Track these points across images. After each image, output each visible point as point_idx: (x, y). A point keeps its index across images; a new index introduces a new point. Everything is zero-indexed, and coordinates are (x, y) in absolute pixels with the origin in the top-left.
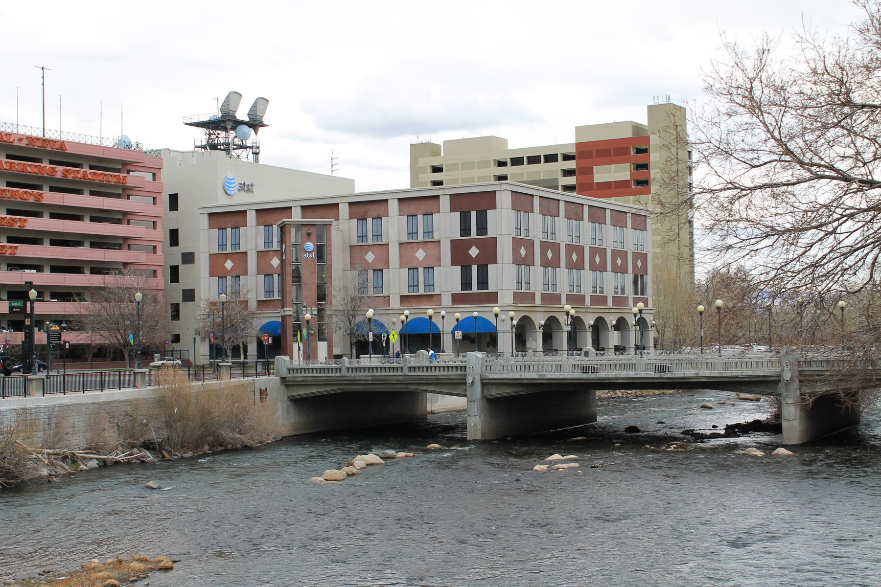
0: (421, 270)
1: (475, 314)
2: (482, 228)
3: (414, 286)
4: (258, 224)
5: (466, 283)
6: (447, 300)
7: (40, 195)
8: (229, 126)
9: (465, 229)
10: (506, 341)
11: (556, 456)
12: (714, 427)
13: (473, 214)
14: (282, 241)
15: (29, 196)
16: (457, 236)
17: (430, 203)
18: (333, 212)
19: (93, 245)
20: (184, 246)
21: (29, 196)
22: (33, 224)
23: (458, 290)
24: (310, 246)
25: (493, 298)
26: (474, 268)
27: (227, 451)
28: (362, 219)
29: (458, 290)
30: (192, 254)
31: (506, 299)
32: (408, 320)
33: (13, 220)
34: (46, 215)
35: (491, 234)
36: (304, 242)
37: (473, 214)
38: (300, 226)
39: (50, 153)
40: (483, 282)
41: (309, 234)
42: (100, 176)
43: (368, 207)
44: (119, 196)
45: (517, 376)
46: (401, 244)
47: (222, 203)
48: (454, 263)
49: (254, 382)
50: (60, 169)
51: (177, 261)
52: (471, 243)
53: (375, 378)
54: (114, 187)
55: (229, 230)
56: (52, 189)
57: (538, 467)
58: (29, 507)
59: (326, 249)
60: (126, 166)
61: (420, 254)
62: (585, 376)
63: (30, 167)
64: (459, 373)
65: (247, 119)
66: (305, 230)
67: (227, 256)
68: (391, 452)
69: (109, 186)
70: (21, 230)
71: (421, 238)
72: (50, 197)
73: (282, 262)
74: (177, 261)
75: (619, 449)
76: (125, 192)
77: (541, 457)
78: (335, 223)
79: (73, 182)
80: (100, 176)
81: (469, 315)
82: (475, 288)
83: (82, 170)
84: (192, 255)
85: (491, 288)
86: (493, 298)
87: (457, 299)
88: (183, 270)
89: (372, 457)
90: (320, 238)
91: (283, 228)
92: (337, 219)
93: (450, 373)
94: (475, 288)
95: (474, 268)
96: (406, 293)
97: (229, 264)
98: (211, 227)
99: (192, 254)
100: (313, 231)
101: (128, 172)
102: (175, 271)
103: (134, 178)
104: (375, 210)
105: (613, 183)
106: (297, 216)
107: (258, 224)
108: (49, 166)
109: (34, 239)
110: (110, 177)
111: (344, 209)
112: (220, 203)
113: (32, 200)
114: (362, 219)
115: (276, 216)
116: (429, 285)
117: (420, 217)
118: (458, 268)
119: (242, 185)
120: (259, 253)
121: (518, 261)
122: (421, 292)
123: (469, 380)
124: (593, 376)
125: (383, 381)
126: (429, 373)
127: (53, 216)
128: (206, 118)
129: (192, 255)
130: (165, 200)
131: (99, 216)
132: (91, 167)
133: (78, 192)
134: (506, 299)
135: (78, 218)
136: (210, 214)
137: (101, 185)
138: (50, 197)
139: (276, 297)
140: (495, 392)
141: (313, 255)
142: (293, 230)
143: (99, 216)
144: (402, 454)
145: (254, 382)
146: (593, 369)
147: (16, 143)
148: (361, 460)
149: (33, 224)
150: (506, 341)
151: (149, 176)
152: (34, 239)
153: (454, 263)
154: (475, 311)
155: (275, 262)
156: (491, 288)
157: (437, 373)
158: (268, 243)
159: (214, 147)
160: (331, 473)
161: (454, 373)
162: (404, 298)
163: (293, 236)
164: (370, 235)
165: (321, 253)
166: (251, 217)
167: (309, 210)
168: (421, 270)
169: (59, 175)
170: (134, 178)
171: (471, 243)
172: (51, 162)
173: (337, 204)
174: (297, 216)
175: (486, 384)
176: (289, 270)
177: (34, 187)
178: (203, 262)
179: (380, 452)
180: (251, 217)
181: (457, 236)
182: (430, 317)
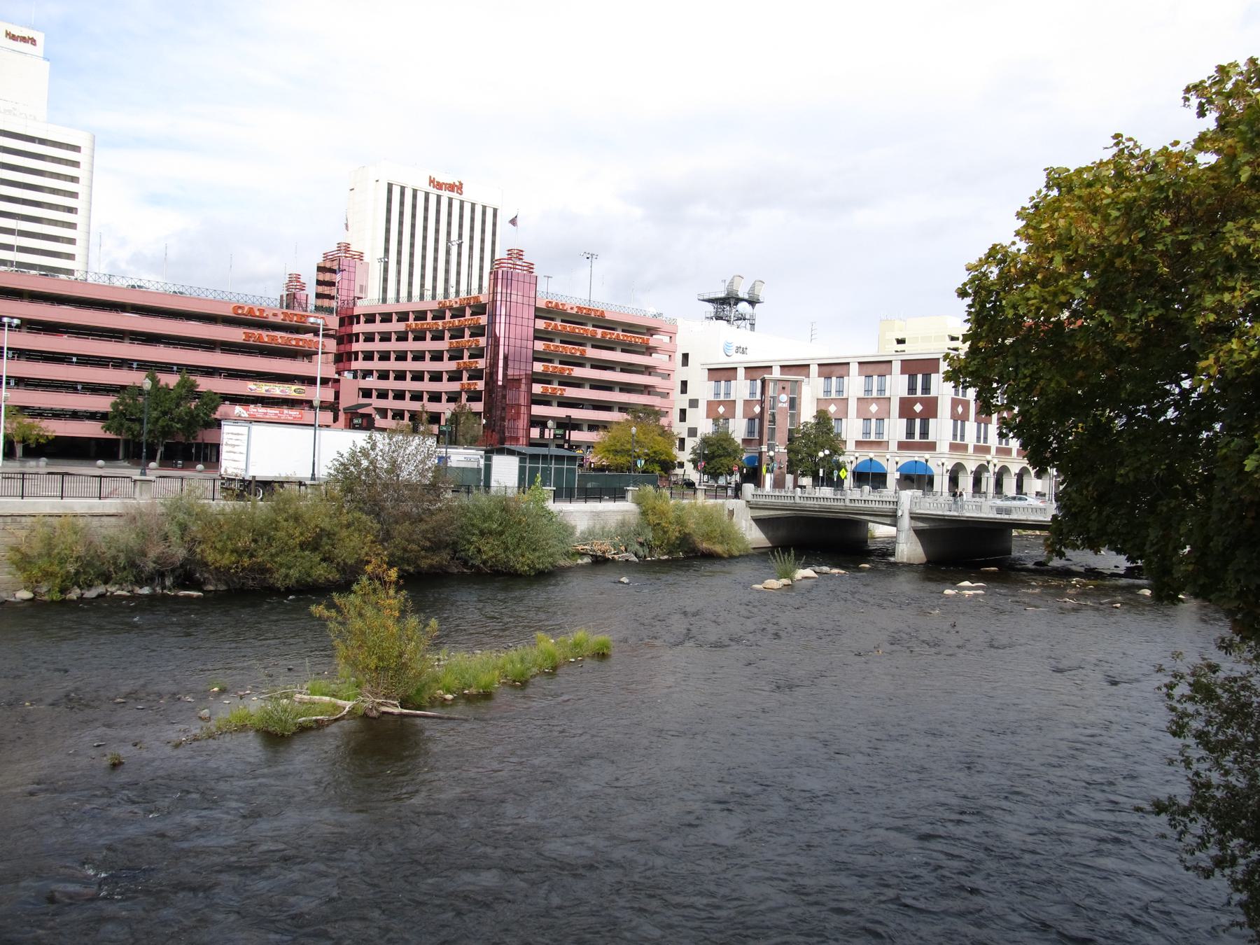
0: (873, 421)
1: (916, 459)
2: (926, 389)
3: (867, 433)
4: (746, 379)
5: (910, 434)
6: (893, 446)
7: (584, 351)
8: (732, 303)
9: (912, 389)
10: (941, 483)
11: (967, 583)
12: (1116, 567)
13: (920, 377)
14: (763, 393)
15: (576, 351)
16: (905, 394)
17: (884, 366)
18: (805, 371)
19: (621, 390)
20: (691, 394)
21: (576, 351)
22: (578, 372)
23: (903, 438)
24: (784, 398)
25: (932, 447)
26: (918, 421)
27: (696, 557)
28: (828, 377)
29: (903, 438)
30: (697, 400)
31: (943, 447)
32: (859, 461)
33: (563, 369)
34: (588, 365)
35: (933, 393)
36: (779, 395)
37: (920, 377)
38: (777, 381)
39: (593, 319)
40: (924, 434)
41: (784, 388)
42: (570, 349)
43: (833, 368)
44: (643, 353)
45: (940, 513)
46: (858, 399)
47: (721, 361)
48: (901, 416)
49: (723, 503)
50: (600, 331)
51: (686, 405)
52: (916, 401)
53: (821, 506)
54: (640, 346)
55: (723, 382)
56: (594, 346)
57: (948, 592)
58: (1031, 849)
59: (797, 401)
60: (651, 331)
61: (874, 408)
62: (999, 516)
63: (578, 329)
64: (891, 506)
65: (746, 297)
66: (780, 385)
67: (720, 403)
68: (825, 569)
69: (636, 345)
70: (569, 377)
71: (875, 394)
72: (591, 353)
73: (762, 409)
74: (686, 405)
75: (606, 500)
76: (649, 350)
77: (954, 583)
78: (806, 380)
79: (610, 341)
80: (570, 349)
81: (912, 459)
82: (917, 438)
83: (616, 333)
84: (697, 401)
85: (931, 438)
86: (932, 447)
87: (902, 446)
88: (689, 412)
89: (808, 572)
90: (793, 391)
91: (764, 382)
92: (808, 376)
93: (884, 506)
94: (917, 438)
95: (918, 421)
96: (861, 439)
97: (721, 410)
98: (710, 379)
99: (697, 400)
100: (788, 386)
101: (652, 335)
102: (683, 412)
103: (654, 341)
104: (838, 370)
105: (93, 442)
106: (776, 373)
107: (746, 379)
108: (591, 328)
109: (578, 383)
110: (637, 339)
111: (814, 370)
112: (720, 361)
113: (578, 354)
114: (828, 377)
115: (760, 372)
116: (879, 433)
117: (875, 378)
118: (905, 420)
119: (738, 348)
120: (746, 402)
121: (955, 417)
122: (873, 438)
123: (899, 513)
124: (1007, 517)
125: (829, 510)
126: (867, 505)
127: (593, 367)
128: (712, 296)
129: (697, 401)
130: (679, 358)
131: (627, 368)
132: (623, 331)
133: (612, 349)
134: (943, 447)
135: (612, 369)
136: (709, 370)
137: (630, 344)
138: (591, 353)
139: (757, 437)
140: (920, 525)
141: (786, 405)
142: (771, 384)
143: (627, 368)
144: (835, 571)
145: (723, 503)
146: (1008, 511)
147: (569, 311)
148: (801, 573)
149: (578, 372)
150: (941, 483)
151: (666, 339)
152: (578, 383)
153: (901, 416)
154: (918, 456)
155: (757, 409)
156: (931, 438)
157: (873, 505)
158: (753, 393)
159: (719, 318)
160: (774, 583)
161: (888, 506)
162: (858, 443)
163: (770, 390)
164: (833, 391)
165: (793, 403)
166: (741, 373)
167: (786, 369)
168: (873, 421)
169: (599, 336)
170: (654, 341)
171: (916, 401)
172: (594, 326)
173: (809, 365)
174: (776, 373)
175: (914, 517)
176: (767, 417)
177: (581, 345)
178: (703, 406)
179: (817, 569)
180: (741, 373)
181: (905, 394)
182: (927, 461)
